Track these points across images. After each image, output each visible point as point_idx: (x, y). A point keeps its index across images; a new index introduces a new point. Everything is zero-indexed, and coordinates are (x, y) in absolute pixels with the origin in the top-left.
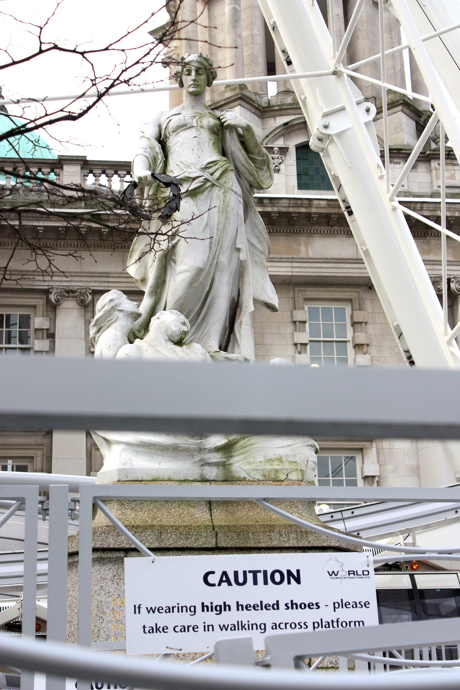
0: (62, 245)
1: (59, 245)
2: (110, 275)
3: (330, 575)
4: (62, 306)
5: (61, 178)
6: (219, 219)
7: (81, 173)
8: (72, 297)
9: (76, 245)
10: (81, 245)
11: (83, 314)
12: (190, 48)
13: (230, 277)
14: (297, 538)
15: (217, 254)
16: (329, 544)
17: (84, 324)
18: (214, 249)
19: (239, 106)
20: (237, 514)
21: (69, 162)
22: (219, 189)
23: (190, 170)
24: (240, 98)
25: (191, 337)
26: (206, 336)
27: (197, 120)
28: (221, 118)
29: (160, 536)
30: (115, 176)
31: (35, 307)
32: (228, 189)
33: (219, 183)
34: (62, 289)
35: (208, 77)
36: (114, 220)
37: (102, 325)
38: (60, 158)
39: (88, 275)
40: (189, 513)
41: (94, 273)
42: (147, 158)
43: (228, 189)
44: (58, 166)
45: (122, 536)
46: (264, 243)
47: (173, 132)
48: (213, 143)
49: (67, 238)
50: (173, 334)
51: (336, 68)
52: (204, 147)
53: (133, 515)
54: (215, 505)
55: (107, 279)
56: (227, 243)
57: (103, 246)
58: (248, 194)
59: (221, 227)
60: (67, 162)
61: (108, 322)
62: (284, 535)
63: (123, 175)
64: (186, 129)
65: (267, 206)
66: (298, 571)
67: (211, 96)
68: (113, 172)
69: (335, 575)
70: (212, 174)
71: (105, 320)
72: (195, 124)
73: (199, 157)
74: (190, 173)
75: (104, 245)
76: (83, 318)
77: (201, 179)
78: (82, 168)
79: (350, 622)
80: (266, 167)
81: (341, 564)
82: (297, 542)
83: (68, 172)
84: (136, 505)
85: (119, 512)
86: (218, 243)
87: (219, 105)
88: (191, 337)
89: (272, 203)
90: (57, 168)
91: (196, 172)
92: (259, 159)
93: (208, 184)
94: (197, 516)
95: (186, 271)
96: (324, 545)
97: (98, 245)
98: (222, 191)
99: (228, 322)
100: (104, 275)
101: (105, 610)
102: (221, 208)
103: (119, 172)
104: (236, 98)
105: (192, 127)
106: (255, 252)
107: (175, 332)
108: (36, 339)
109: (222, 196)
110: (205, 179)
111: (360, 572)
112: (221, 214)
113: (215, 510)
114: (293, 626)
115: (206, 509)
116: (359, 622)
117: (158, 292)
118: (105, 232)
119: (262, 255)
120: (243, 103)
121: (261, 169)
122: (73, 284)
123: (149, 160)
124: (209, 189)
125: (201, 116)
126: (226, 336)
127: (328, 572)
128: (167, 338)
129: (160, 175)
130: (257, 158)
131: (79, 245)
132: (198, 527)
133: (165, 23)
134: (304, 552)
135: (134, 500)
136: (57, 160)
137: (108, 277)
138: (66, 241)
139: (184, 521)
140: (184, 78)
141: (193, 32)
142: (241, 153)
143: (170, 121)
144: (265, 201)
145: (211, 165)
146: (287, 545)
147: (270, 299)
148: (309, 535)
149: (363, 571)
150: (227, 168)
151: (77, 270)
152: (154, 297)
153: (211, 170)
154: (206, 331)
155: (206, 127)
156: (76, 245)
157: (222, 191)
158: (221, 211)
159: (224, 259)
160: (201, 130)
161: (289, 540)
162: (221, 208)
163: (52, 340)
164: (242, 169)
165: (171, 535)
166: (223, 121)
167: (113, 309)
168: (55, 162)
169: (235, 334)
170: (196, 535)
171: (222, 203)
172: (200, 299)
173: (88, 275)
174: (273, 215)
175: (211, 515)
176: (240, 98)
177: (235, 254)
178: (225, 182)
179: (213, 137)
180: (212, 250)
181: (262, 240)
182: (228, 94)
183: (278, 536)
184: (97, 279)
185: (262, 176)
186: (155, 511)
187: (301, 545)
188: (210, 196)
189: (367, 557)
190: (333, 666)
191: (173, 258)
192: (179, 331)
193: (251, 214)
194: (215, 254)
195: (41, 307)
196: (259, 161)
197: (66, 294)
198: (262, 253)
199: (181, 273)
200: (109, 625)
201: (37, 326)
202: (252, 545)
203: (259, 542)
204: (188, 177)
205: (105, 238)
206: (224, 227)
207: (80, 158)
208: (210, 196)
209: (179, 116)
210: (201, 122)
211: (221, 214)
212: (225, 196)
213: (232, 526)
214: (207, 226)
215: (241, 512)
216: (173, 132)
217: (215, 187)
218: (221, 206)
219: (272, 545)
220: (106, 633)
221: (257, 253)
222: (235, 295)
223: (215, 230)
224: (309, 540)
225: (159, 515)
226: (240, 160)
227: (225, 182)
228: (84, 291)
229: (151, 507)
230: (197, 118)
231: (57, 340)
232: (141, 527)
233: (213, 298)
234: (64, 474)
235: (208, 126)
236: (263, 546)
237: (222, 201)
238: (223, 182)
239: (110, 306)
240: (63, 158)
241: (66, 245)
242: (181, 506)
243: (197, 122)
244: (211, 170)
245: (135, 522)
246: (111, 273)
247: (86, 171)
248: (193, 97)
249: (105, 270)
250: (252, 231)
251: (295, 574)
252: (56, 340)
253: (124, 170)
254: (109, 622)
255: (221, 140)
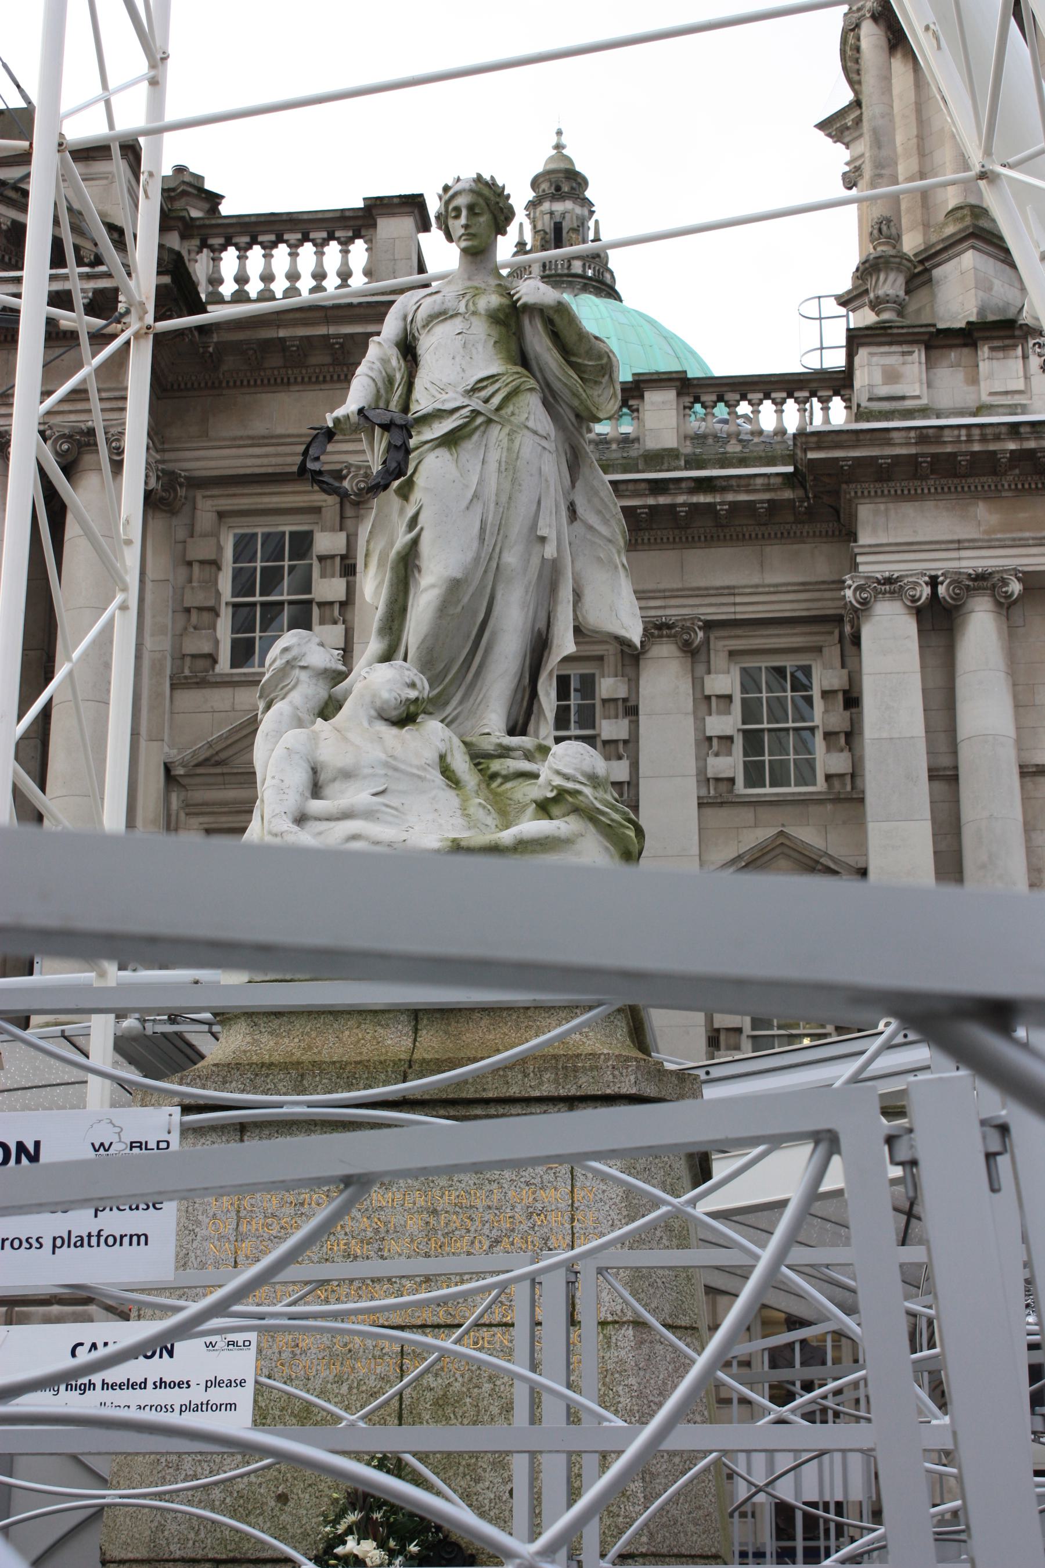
0: (646, 541)
1: (640, 541)
2: (736, 591)
3: (96, 1151)
4: (650, 655)
5: (641, 416)
6: (499, 484)
7: (678, 404)
8: (668, 636)
9: (671, 539)
10: (681, 538)
11: (689, 667)
12: (879, 148)
13: (527, 592)
14: (556, 1081)
15: (497, 550)
16: (616, 1090)
17: (691, 685)
18: (490, 541)
19: (971, 251)
20: (464, 1038)
21: (654, 385)
22: (499, 427)
23: (445, 397)
24: (972, 235)
25: (455, 709)
26: (482, 706)
27: (468, 301)
28: (512, 292)
29: (302, 1080)
30: (788, 400)
31: (600, 658)
32: (518, 427)
33: (501, 417)
34: (649, 622)
35: (495, 218)
36: (738, 486)
37: (272, 696)
38: (637, 378)
39: (696, 593)
40: (374, 1038)
41: (707, 589)
42: (374, 380)
43: (518, 427)
44: (635, 394)
45: (231, 1082)
46: (613, 523)
47: (424, 327)
48: (496, 342)
49: (655, 526)
50: (385, 706)
51: (983, 166)
52: (474, 351)
53: (272, 1043)
54: (425, 1022)
55: (731, 599)
56: (517, 528)
57: (722, 537)
58: (576, 433)
59: (504, 499)
60: (650, 385)
61: (282, 689)
62: (532, 1075)
63: (712, 404)
64: (446, 319)
65: (1028, 439)
66: (37, 1144)
67: (924, 235)
68: (738, 397)
69: (106, 1150)
70: (486, 401)
71: (277, 686)
72: (462, 310)
73: (463, 370)
74: (444, 402)
75: (725, 536)
76: (690, 675)
77: (465, 412)
78: (679, 394)
79: (122, 1237)
80: (607, 377)
81: (118, 1130)
82: (556, 1088)
83: (652, 403)
84: (280, 1025)
85: (248, 1039)
86: (499, 530)
87: (933, 251)
88: (455, 709)
89: (1038, 433)
90: (633, 398)
91: (455, 399)
92: (590, 363)
93: (480, 420)
94: (389, 1042)
95: (433, 586)
96: (608, 1091)
97: (712, 537)
98: (506, 430)
99: (527, 676)
100: (726, 591)
101: (200, 1217)
102: (503, 464)
103: (749, 396)
104: (963, 234)
105: (457, 315)
106: (597, 540)
107: (387, 702)
108: (605, 718)
109: (505, 441)
110: (473, 411)
111: (152, 1145)
112: (504, 474)
113: (424, 1032)
114: (16, 1244)
115: (408, 1029)
116: (139, 1237)
117: (395, 627)
118: (722, 510)
119: (611, 546)
120: (979, 244)
121: (597, 383)
122: (669, 612)
123: (376, 385)
124: (482, 428)
125: (477, 292)
126: (525, 704)
127: (93, 1144)
128: (373, 713)
129: (373, 412)
130: (586, 362)
131: (677, 540)
132: (381, 1062)
133: (847, 103)
134: (571, 1109)
135: (277, 1014)
136: (631, 382)
137: (734, 594)
138: (652, 533)
139: (361, 1053)
140: (451, 223)
141: (883, 117)
142: (552, 356)
143: (418, 307)
144: (1022, 430)
145: (485, 383)
146: (537, 1093)
147: (623, 628)
148: (579, 1074)
149: (158, 1142)
150: (518, 387)
151: (675, 586)
152: (387, 638)
153: (484, 394)
154: (481, 696)
155: (483, 312)
156: (671, 539)
157: (506, 430)
158: (503, 468)
159: (511, 558)
160: (474, 320)
161: (541, 1083)
162: (503, 464)
163: (634, 718)
164: (557, 385)
165: (321, 1079)
166: (515, 298)
167: (290, 665)
168: (630, 386)
169: (539, 700)
170: (367, 1079)
171: (505, 454)
172: (469, 637)
173: (696, 593)
174: (1039, 455)
175: (415, 1040)
176: (972, 235)
177: (537, 548)
178: (513, 414)
179: (495, 332)
180: (486, 543)
181: (608, 517)
182: (950, 230)
183: (520, 1076)
184: (713, 600)
185: (599, 396)
186: (314, 1034)
187: (562, 1092)
188: (484, 443)
189: (170, 1115)
190: (617, 1318)
191: (417, 562)
192: (396, 699)
193: (585, 470)
194: (493, 549)
195: (612, 659)
196: (589, 368)
197: (656, 632)
198: (610, 541)
199: (426, 590)
200: (205, 1244)
201: (605, 695)
202: (470, 1096)
203: (484, 1090)
204: (440, 410)
205: (724, 522)
206: (510, 498)
207: (674, 376)
208: (484, 443)
209: (435, 297)
210: (474, 304)
211: (504, 474)
212: (511, 441)
213: (446, 1060)
214: (475, 500)
215: (473, 1033)
216: (424, 327)
217: (493, 425)
218: (504, 459)
219: (508, 1094)
220: (199, 1260)
221: (602, 543)
222: (542, 624)
223: (492, 506)
224: (580, 1083)
225: (319, 1043)
226: (551, 369)
227: (513, 414)
228: (688, 624)
229: (308, 1029)
230: (468, 297)
231: (642, 718)
232: (276, 1066)
233: (494, 634)
234: (61, 973)
235: (487, 310)
236: (491, 1095)
237: (505, 450)
238: (509, 413)
239: (284, 661)
240: (642, 378)
241: (652, 541)
242: (363, 1026)
243: (467, 306)
244: (484, 394)
245: (270, 1056)
246: (738, 587)
247: (687, 400)
248: (469, 258)
249: (727, 582)
250: (589, 501)
251: (31, 1150)
252: (641, 718)
253: (759, 391)
254: (205, 1239)
255: (514, 334)
